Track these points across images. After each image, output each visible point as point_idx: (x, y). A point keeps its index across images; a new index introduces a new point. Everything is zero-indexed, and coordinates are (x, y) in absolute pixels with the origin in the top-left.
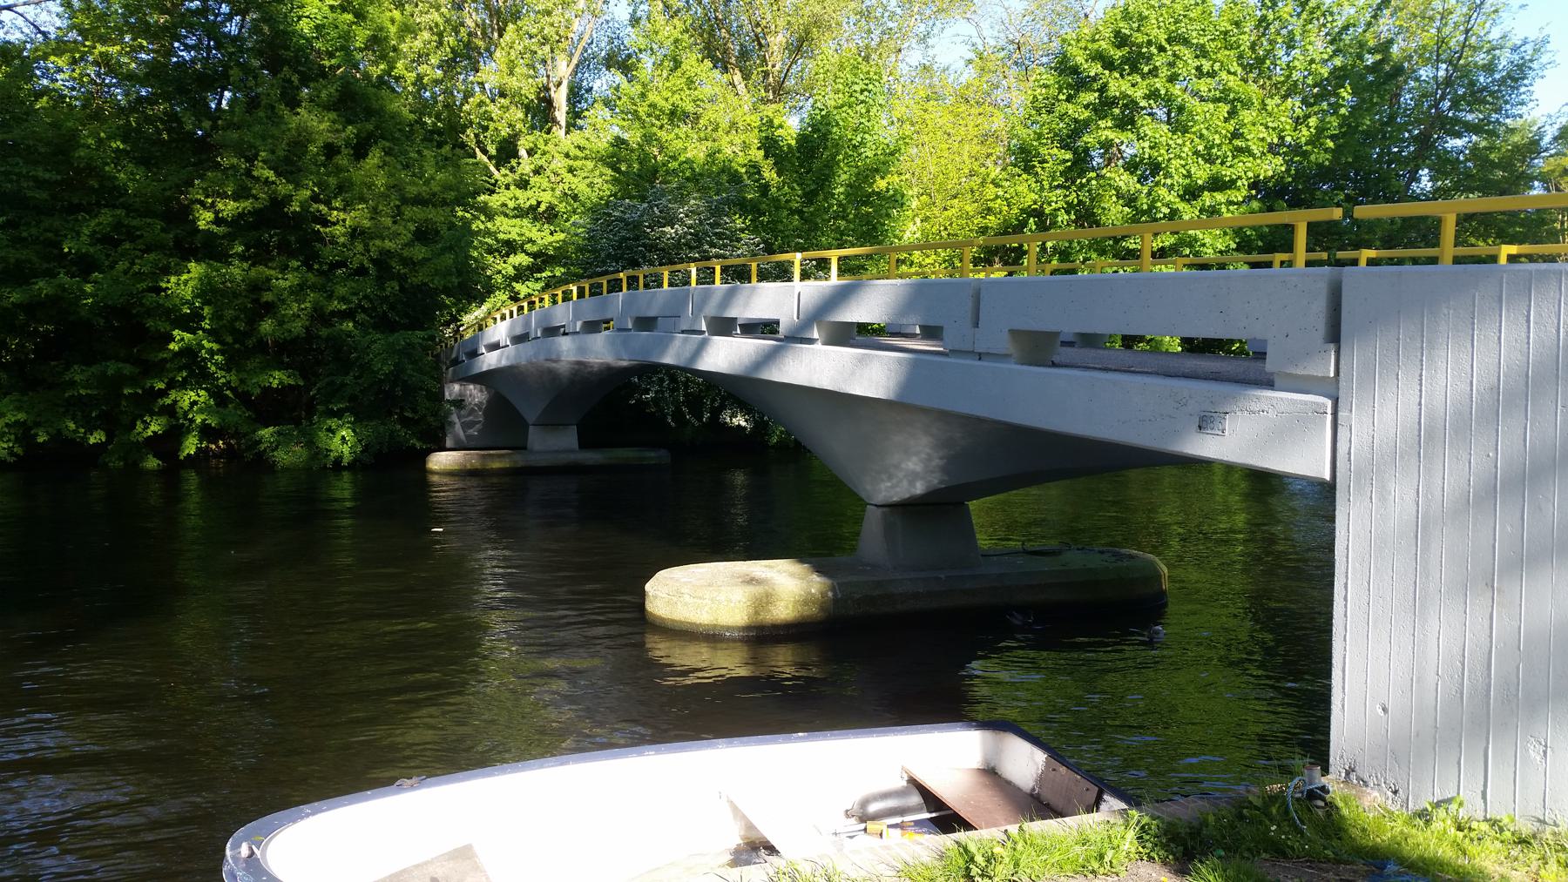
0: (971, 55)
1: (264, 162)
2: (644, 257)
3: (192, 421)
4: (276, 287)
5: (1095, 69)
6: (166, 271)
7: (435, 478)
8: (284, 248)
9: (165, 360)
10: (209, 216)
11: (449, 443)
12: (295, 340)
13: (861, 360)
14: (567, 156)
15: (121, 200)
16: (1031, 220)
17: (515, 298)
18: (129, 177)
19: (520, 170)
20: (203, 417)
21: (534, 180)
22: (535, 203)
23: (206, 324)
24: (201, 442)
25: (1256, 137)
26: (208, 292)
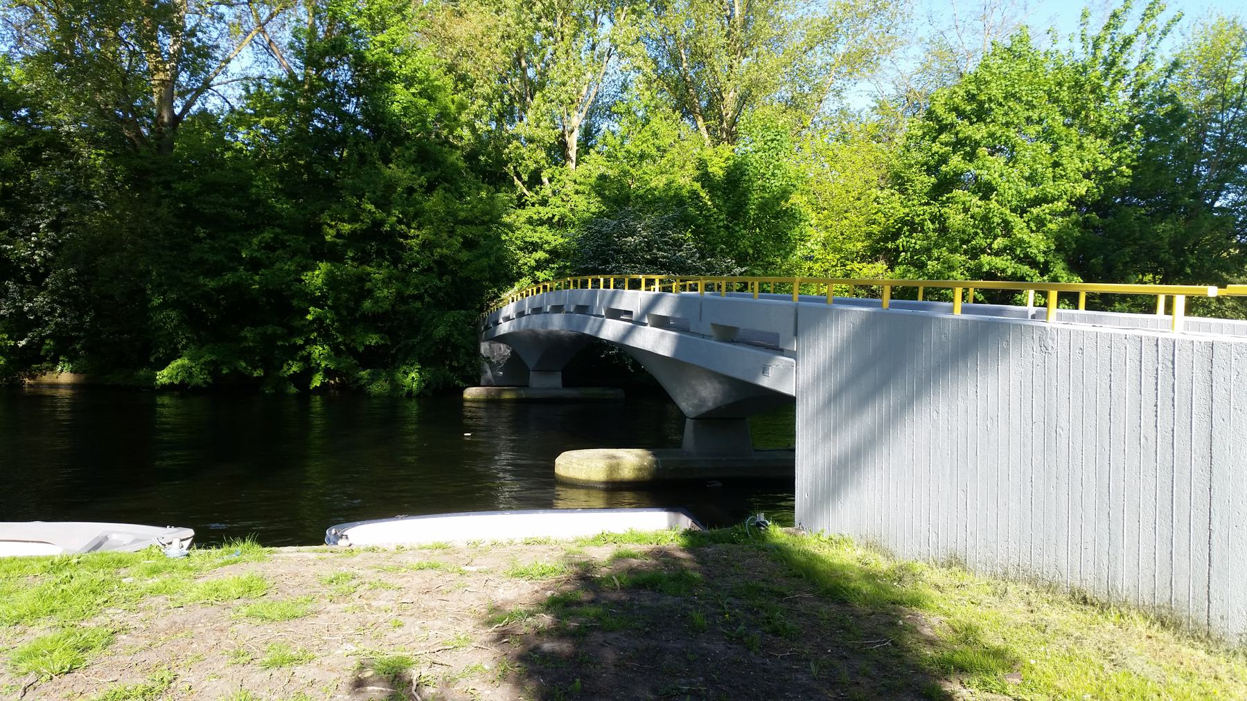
0: (874, 104)
1: (369, 199)
2: (613, 258)
3: (319, 365)
4: (374, 278)
5: (951, 118)
6: (306, 268)
7: (467, 404)
8: (380, 253)
9: (304, 326)
10: (332, 232)
11: (482, 382)
12: (386, 313)
13: (662, 335)
14: (575, 182)
15: (277, 222)
16: (905, 228)
17: (536, 282)
18: (283, 206)
19: (542, 193)
20: (326, 363)
21: (552, 200)
22: (551, 216)
23: (329, 303)
24: (324, 378)
25: (1072, 165)
26: (331, 280)
